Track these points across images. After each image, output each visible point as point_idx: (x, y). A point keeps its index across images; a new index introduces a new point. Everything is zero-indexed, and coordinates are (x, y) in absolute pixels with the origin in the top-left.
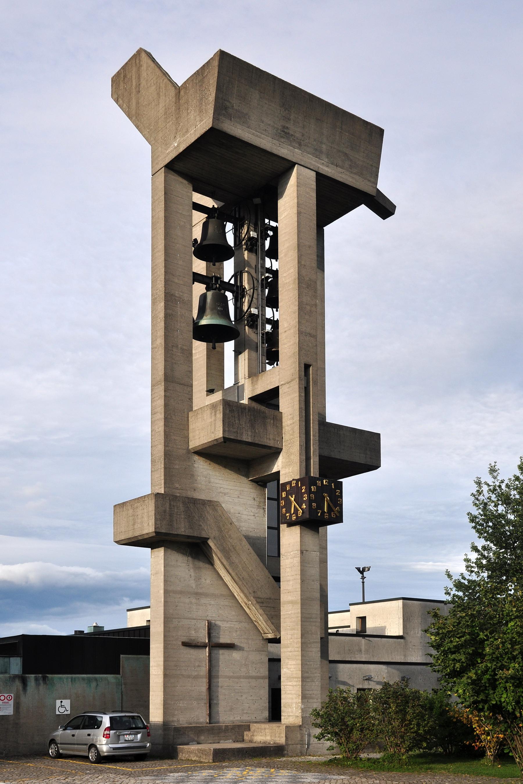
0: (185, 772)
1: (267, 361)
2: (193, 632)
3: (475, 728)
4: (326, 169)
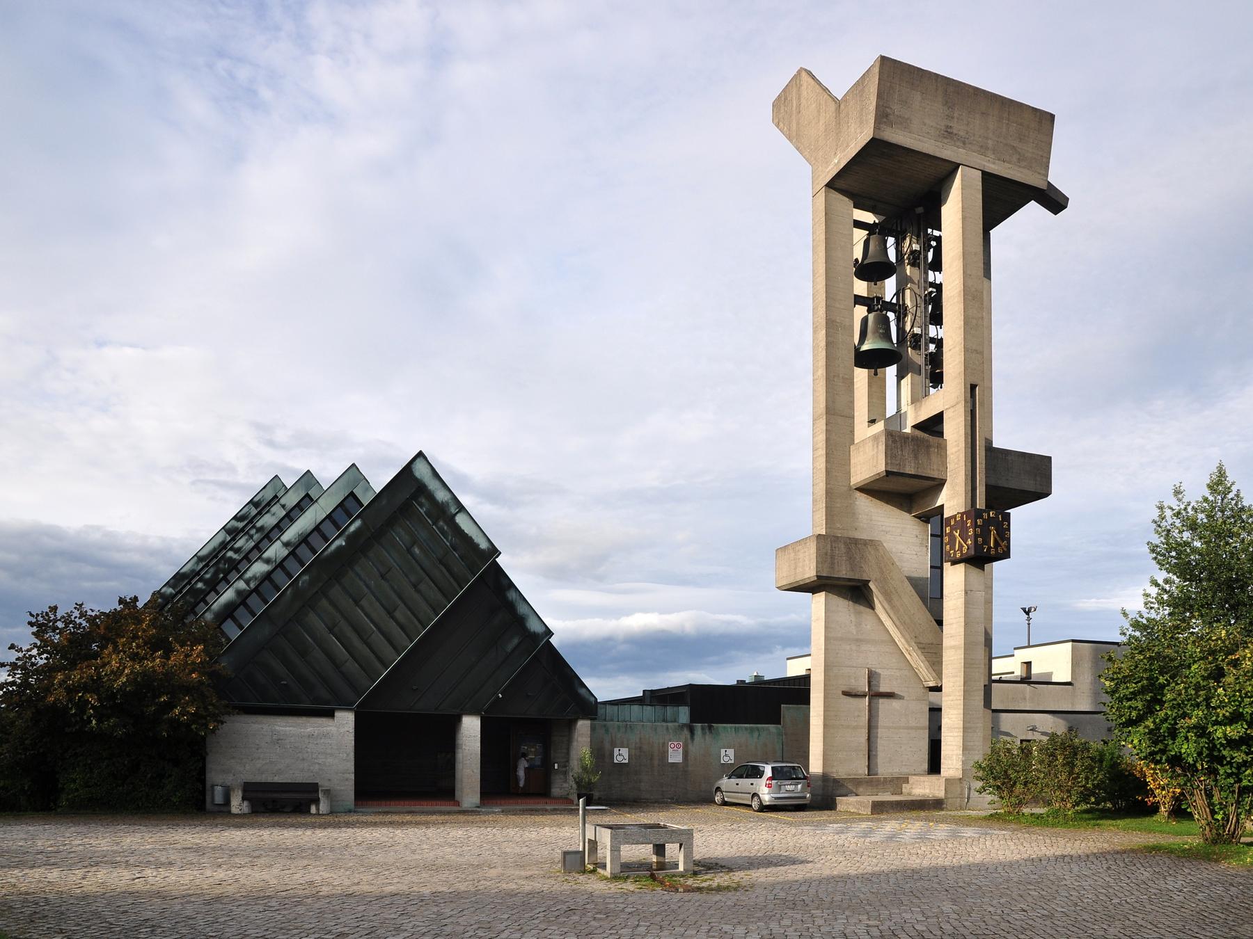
0: (844, 824)
1: (931, 384)
2: (853, 681)
3: (1149, 782)
4: (993, 166)
